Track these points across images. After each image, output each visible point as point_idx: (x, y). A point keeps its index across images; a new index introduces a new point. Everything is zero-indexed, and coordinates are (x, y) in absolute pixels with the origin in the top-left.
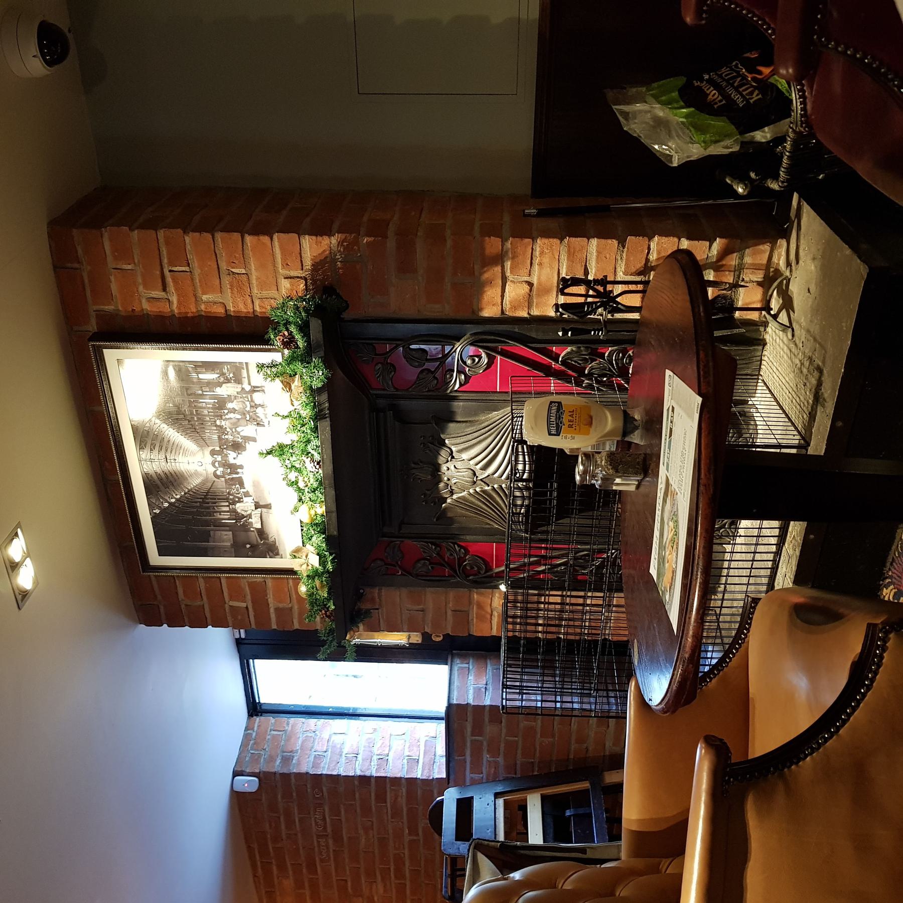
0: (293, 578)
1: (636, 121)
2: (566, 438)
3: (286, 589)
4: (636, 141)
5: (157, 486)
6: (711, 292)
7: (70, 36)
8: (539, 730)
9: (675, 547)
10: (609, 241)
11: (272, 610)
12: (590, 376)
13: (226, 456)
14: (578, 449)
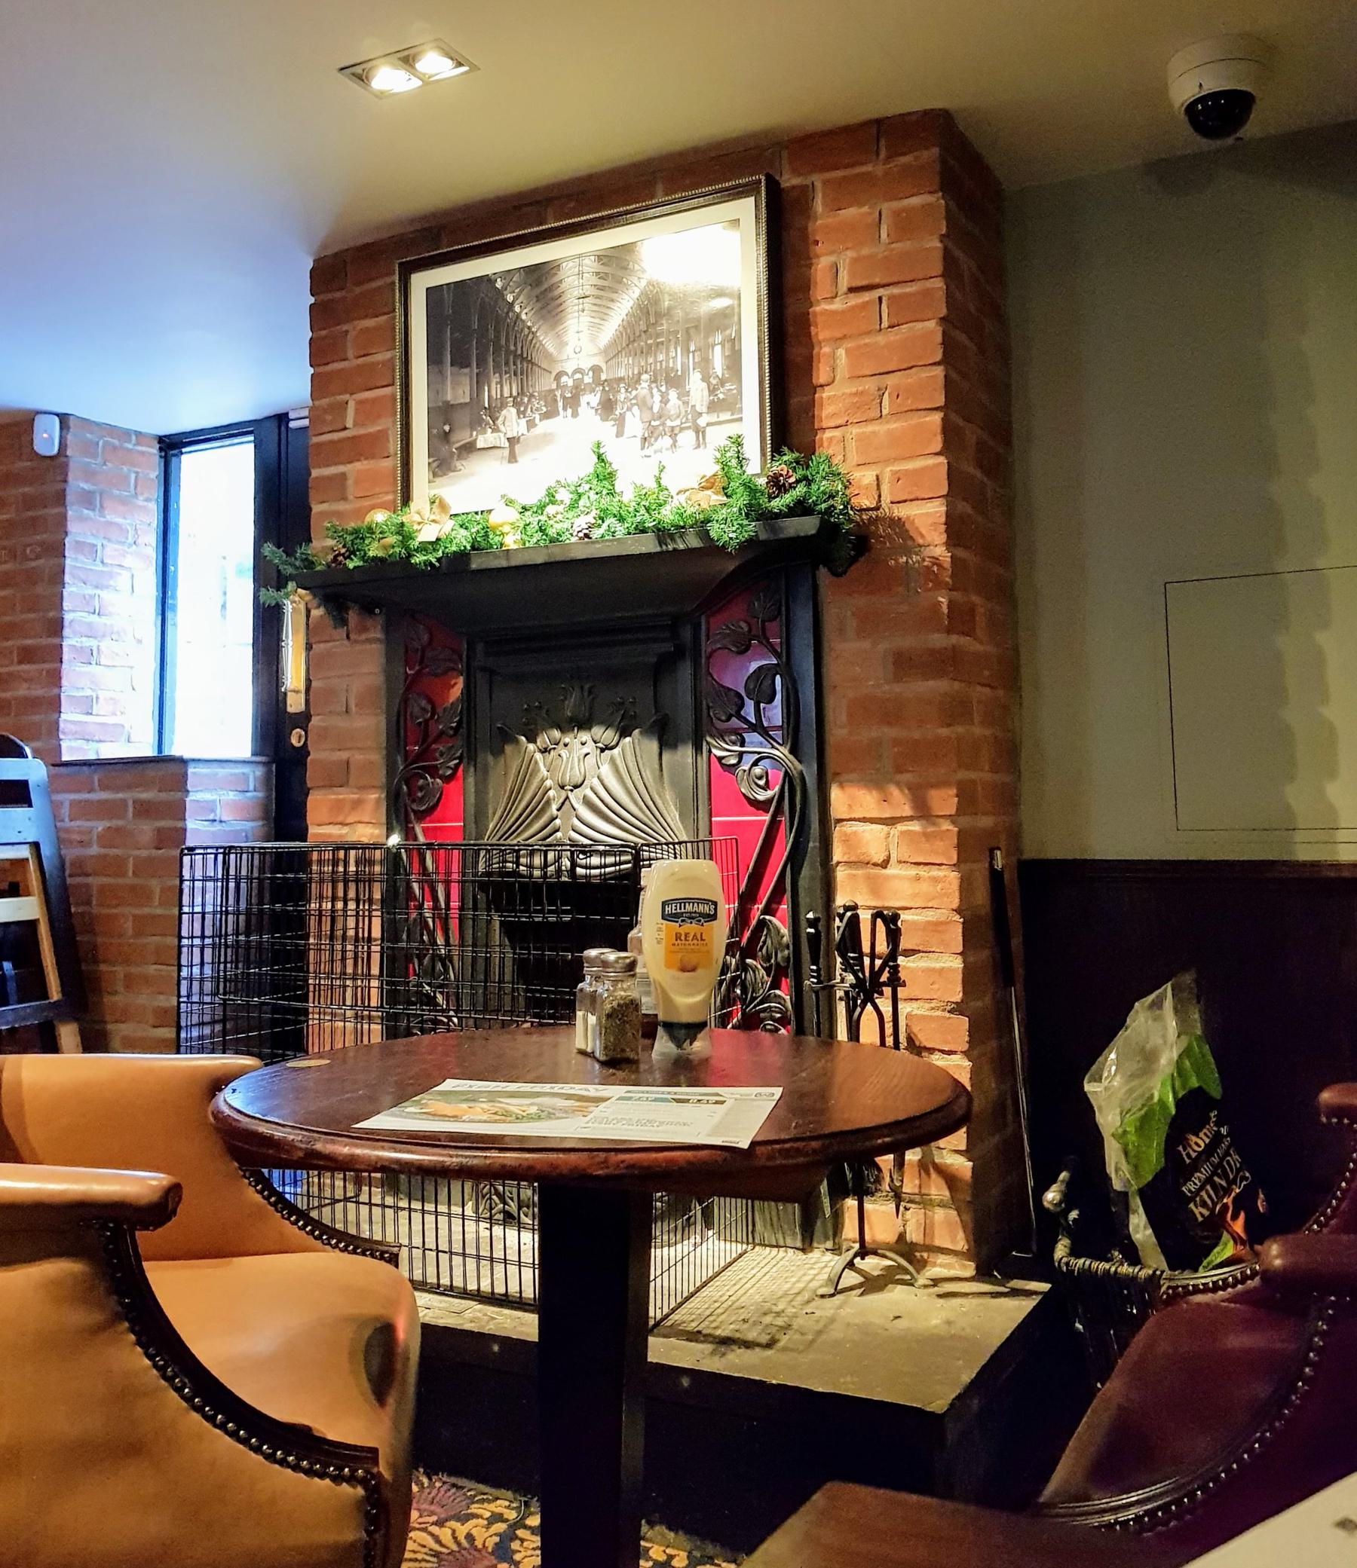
0: (395, 501)
1: (1150, 1022)
2: (660, 930)
3: (377, 490)
4: (1115, 1023)
5: (538, 282)
6: (886, 1161)
7: (1230, 141)
8: (146, 910)
9: (498, 1117)
10: (959, 988)
11: (341, 469)
12: (743, 967)
13: (593, 391)
14: (640, 952)
